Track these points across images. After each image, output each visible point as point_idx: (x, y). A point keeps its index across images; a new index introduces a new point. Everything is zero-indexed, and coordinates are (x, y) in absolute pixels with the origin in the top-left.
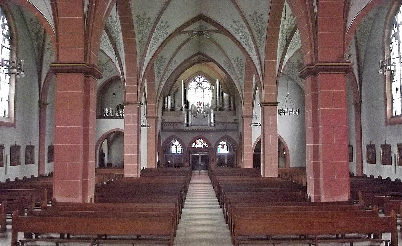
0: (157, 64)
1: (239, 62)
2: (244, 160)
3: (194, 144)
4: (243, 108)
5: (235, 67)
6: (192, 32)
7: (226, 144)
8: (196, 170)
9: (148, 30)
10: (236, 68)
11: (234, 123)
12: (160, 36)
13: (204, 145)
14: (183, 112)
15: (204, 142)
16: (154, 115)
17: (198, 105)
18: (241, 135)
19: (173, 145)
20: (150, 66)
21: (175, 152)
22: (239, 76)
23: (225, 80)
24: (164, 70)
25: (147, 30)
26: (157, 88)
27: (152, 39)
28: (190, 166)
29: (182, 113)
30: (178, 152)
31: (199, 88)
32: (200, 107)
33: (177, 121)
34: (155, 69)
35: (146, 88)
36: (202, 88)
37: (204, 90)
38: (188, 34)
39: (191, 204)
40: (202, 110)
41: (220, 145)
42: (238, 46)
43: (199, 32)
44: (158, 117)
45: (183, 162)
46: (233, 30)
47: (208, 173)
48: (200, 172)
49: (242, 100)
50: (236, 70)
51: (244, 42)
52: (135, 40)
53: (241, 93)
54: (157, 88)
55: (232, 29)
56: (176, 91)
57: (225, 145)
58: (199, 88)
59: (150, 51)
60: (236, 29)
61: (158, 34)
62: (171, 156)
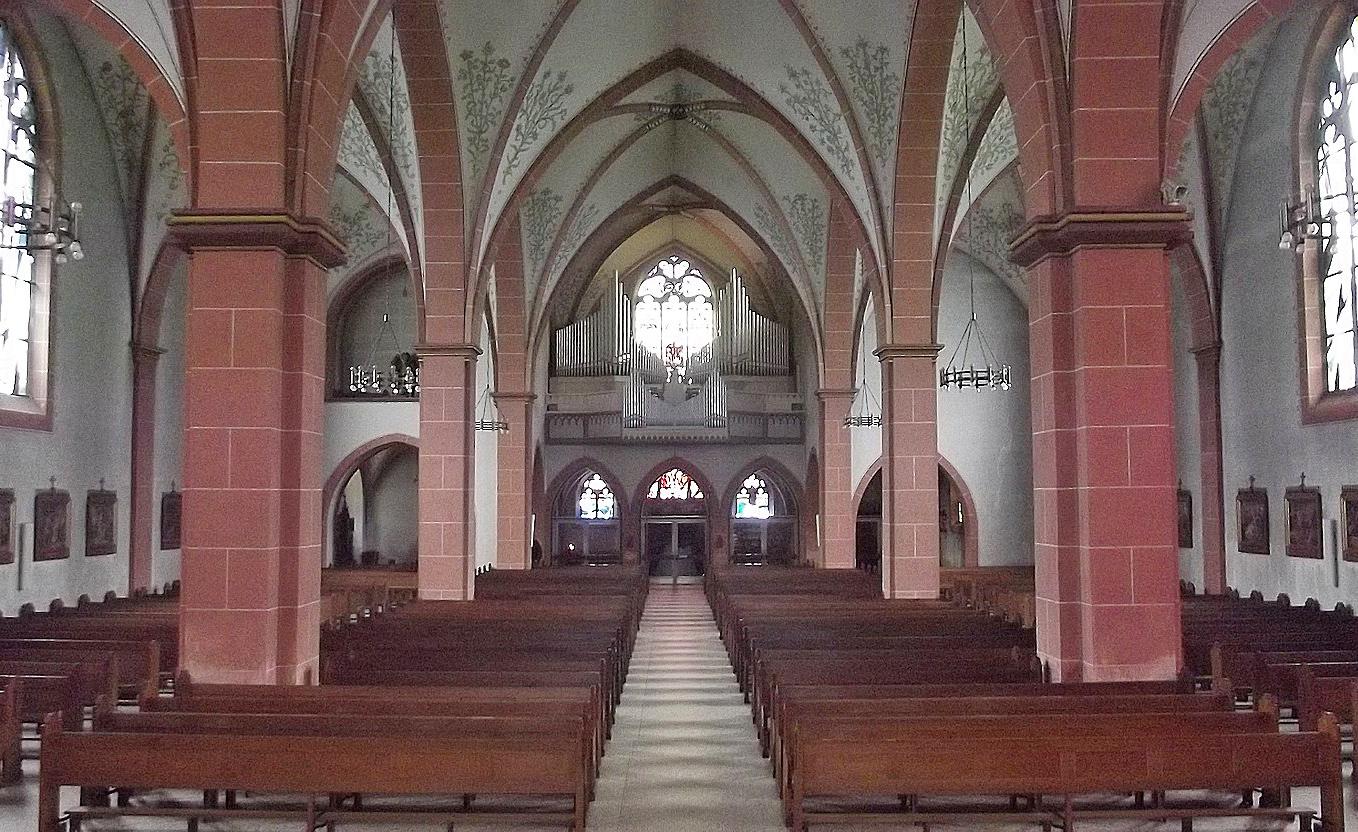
0: (530, 216)
1: (807, 211)
2: (823, 542)
3: (655, 488)
4: (821, 364)
5: (793, 228)
6: (650, 110)
7: (763, 485)
8: (663, 575)
9: (501, 100)
10: (797, 229)
11: (792, 415)
12: (542, 123)
13: (689, 491)
14: (618, 378)
15: (689, 482)
16: (520, 391)
17: (669, 355)
18: (813, 457)
19: (583, 490)
20: (506, 224)
21: (592, 516)
22: (808, 258)
23: (761, 272)
24: (554, 235)
25: (496, 103)
26: (529, 297)
27: (513, 133)
28: (643, 561)
29: (613, 382)
30: (600, 515)
31: (674, 299)
32: (677, 361)
33: (598, 410)
34: (525, 233)
35: (493, 298)
36: (682, 298)
37: (691, 305)
38: (634, 115)
39: (647, 692)
40: (682, 371)
41: (744, 491)
42: (805, 156)
43: (672, 107)
44: (533, 397)
45: (617, 547)
46: (788, 102)
47: (702, 587)
48: (675, 581)
49: (818, 339)
50: (799, 237)
51: (823, 142)
52: (456, 136)
53: (815, 314)
54: (529, 297)
55: (785, 97)
56: (596, 309)
57: (761, 491)
58: (674, 299)
59: (507, 172)
60: (796, 99)
61: (535, 117)
62: (578, 527)
